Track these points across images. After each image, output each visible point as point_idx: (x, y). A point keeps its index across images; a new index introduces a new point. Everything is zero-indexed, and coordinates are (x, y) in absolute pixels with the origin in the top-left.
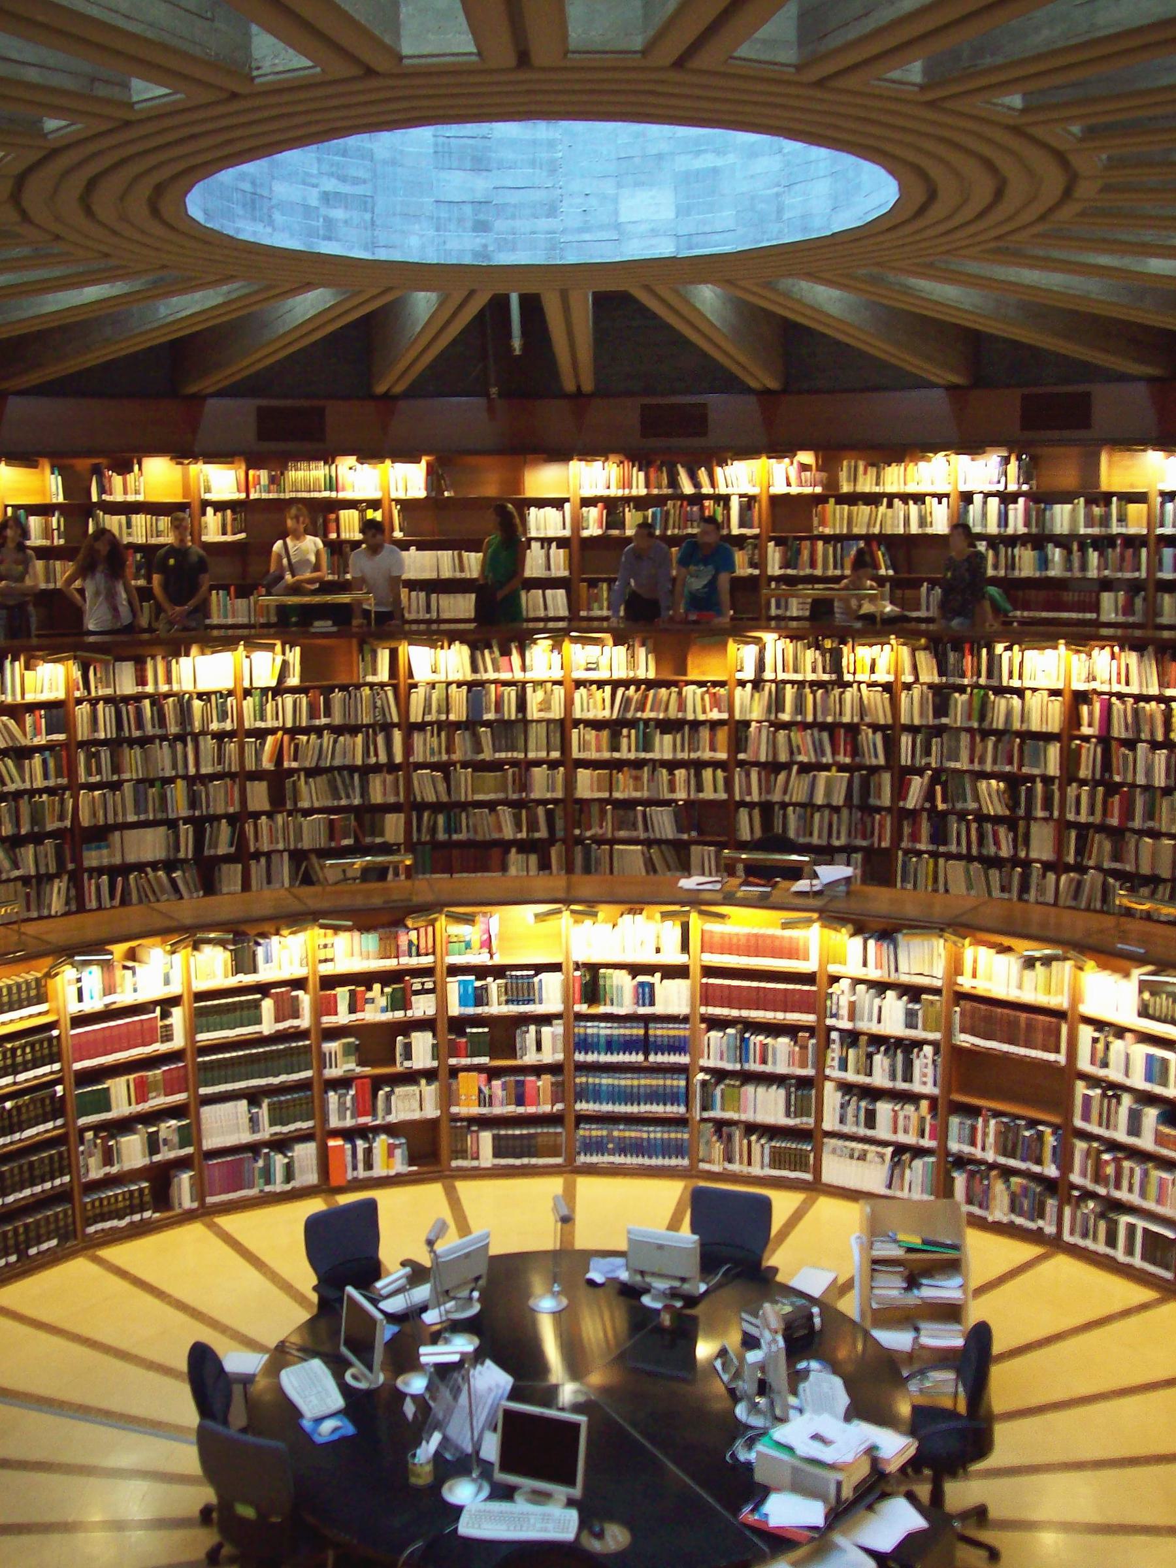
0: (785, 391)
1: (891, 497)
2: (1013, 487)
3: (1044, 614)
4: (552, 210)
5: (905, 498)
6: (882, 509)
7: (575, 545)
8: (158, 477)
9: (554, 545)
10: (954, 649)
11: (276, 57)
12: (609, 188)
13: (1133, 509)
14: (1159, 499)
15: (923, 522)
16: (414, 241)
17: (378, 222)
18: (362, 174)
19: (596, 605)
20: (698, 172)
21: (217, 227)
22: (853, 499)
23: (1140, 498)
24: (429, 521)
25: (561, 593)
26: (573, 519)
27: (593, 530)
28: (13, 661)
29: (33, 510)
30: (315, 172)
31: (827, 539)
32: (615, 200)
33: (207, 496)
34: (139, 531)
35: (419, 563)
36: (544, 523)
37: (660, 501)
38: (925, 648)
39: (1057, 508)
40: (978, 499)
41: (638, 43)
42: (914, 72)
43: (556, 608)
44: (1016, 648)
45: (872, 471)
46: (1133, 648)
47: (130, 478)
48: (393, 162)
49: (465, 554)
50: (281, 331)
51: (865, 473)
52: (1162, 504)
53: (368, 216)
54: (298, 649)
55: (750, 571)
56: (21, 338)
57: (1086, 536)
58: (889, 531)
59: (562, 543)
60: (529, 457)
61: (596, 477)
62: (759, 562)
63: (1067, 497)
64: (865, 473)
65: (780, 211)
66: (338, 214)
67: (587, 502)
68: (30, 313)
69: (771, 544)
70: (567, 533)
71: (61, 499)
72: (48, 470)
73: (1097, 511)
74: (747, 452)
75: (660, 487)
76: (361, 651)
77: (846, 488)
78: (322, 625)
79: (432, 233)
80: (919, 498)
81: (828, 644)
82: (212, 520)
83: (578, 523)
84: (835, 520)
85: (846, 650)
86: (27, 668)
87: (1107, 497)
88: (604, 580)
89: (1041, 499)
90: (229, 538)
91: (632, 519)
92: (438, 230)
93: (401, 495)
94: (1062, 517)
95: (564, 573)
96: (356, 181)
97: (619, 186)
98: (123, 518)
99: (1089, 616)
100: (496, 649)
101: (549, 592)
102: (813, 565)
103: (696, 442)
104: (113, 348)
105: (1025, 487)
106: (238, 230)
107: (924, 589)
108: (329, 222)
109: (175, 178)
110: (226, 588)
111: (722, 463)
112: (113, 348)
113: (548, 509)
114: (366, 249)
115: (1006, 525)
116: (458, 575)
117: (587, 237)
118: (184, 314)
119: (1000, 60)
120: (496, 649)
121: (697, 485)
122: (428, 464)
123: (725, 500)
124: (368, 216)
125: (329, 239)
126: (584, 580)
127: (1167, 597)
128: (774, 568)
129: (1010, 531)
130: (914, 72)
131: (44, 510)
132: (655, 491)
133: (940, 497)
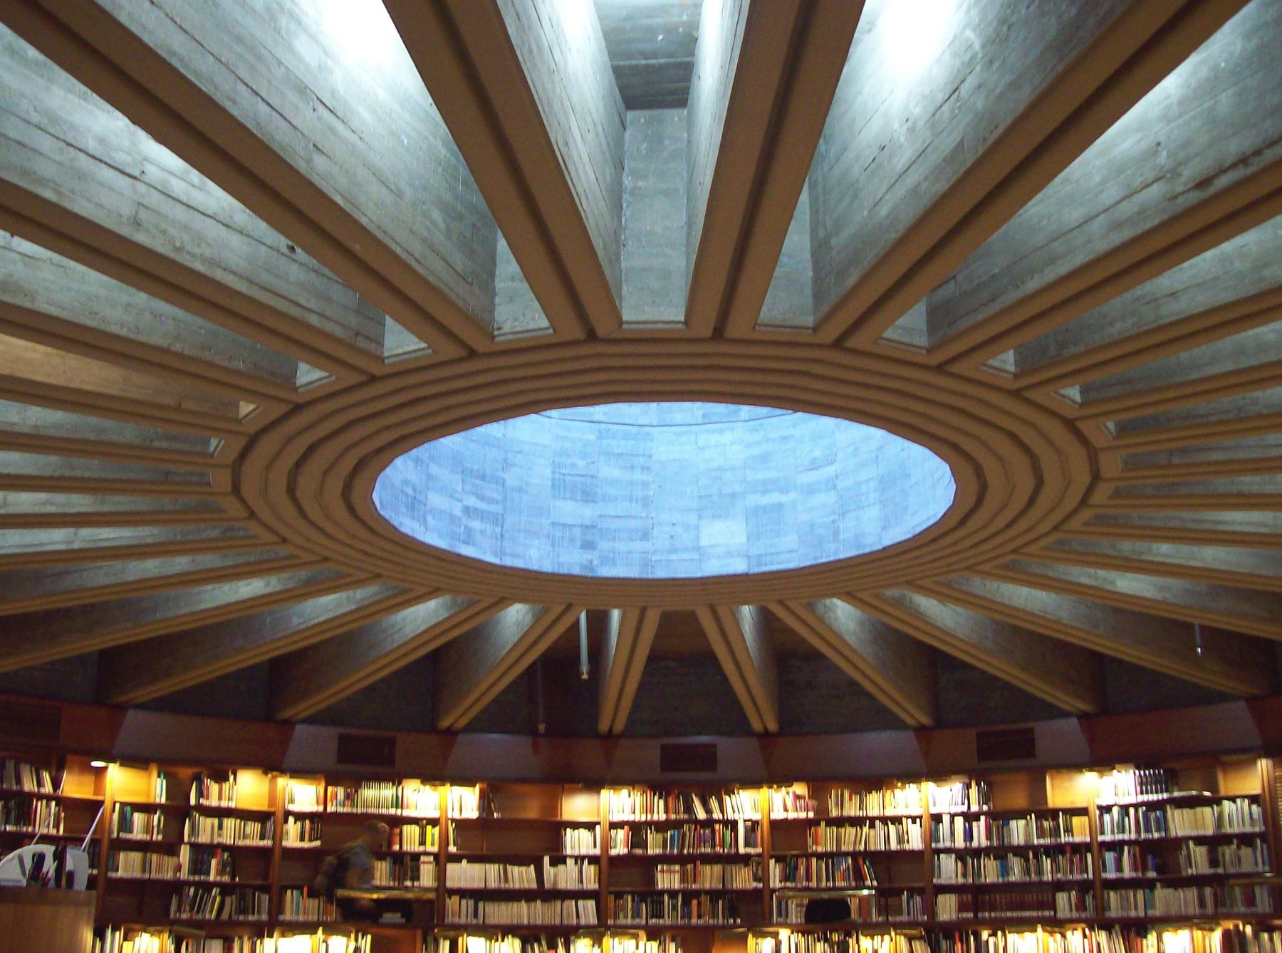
0: (780, 734)
1: (872, 821)
2: (974, 808)
3: (1009, 914)
4: (645, 536)
5: (885, 820)
6: (866, 829)
7: (604, 862)
8: (248, 788)
9: (586, 862)
10: (946, 937)
11: (515, 320)
12: (692, 519)
13: (1076, 821)
14: (1098, 812)
15: (900, 840)
16: (533, 553)
17: (507, 536)
18: (495, 496)
19: (621, 915)
20: (765, 508)
21: (387, 517)
22: (840, 822)
23: (1083, 812)
24: (476, 839)
25: (591, 904)
26: (602, 838)
27: (620, 849)
28: (114, 931)
29: (138, 807)
30: (460, 489)
31: (820, 856)
32: (697, 528)
33: (291, 807)
34: (230, 832)
35: (464, 874)
36: (578, 842)
37: (677, 825)
38: (920, 938)
39: (1013, 823)
40: (946, 819)
41: (810, 321)
42: (1007, 360)
43: (586, 916)
44: (999, 933)
45: (856, 799)
46: (1101, 928)
47: (226, 786)
48: (520, 490)
49: (509, 868)
50: (389, 648)
51: (851, 799)
52: (1101, 816)
53: (498, 530)
54: (369, 937)
55: (755, 884)
56: (168, 636)
57: (1040, 846)
58: (872, 848)
59: (593, 860)
60: (566, 786)
61: (621, 804)
62: (763, 877)
63: (1021, 814)
64: (851, 799)
65: (836, 533)
66: (476, 525)
67: (614, 825)
68: (186, 610)
69: (772, 862)
70: (597, 851)
71: (163, 800)
72: (155, 774)
73: (1046, 824)
74: (754, 783)
75: (677, 812)
76: (425, 941)
77: (834, 813)
78: (389, 917)
79: (549, 547)
80: (897, 820)
81: (835, 937)
82: (292, 827)
83: (607, 844)
84: (826, 839)
85: (852, 941)
86: (125, 939)
87: (1054, 814)
88: (628, 893)
89: (999, 817)
90: (306, 845)
91: (653, 838)
92: (553, 545)
93: (457, 816)
94: (1019, 831)
95: (593, 886)
96: (491, 501)
97: (700, 517)
98: (216, 821)
99: (1047, 913)
100: (544, 943)
101: (581, 903)
102: (808, 878)
103: (703, 776)
104: (244, 656)
105: (985, 808)
106: (401, 523)
107: (904, 897)
108: (468, 530)
109: (379, 451)
110: (300, 888)
111: (730, 792)
112: (244, 656)
113: (582, 830)
114: (496, 554)
115: (971, 839)
116: (503, 886)
117: (674, 557)
118: (316, 621)
119: (1082, 348)
120: (544, 943)
121: (708, 811)
122: (481, 791)
123: (734, 824)
124: (498, 530)
125: (468, 543)
126: (611, 893)
127: (1112, 894)
128: (775, 881)
129: (975, 844)
130: (1007, 360)
131: (148, 808)
132: (673, 817)
133: (914, 819)
